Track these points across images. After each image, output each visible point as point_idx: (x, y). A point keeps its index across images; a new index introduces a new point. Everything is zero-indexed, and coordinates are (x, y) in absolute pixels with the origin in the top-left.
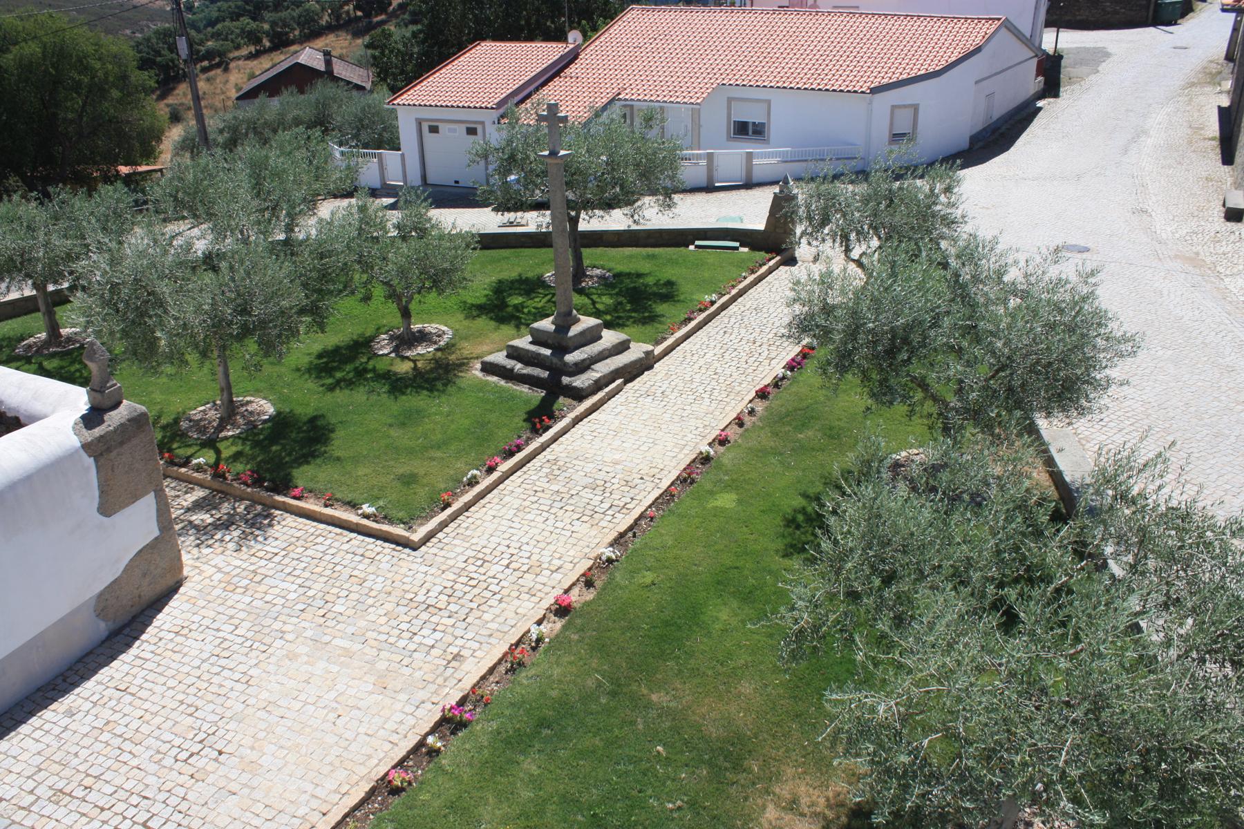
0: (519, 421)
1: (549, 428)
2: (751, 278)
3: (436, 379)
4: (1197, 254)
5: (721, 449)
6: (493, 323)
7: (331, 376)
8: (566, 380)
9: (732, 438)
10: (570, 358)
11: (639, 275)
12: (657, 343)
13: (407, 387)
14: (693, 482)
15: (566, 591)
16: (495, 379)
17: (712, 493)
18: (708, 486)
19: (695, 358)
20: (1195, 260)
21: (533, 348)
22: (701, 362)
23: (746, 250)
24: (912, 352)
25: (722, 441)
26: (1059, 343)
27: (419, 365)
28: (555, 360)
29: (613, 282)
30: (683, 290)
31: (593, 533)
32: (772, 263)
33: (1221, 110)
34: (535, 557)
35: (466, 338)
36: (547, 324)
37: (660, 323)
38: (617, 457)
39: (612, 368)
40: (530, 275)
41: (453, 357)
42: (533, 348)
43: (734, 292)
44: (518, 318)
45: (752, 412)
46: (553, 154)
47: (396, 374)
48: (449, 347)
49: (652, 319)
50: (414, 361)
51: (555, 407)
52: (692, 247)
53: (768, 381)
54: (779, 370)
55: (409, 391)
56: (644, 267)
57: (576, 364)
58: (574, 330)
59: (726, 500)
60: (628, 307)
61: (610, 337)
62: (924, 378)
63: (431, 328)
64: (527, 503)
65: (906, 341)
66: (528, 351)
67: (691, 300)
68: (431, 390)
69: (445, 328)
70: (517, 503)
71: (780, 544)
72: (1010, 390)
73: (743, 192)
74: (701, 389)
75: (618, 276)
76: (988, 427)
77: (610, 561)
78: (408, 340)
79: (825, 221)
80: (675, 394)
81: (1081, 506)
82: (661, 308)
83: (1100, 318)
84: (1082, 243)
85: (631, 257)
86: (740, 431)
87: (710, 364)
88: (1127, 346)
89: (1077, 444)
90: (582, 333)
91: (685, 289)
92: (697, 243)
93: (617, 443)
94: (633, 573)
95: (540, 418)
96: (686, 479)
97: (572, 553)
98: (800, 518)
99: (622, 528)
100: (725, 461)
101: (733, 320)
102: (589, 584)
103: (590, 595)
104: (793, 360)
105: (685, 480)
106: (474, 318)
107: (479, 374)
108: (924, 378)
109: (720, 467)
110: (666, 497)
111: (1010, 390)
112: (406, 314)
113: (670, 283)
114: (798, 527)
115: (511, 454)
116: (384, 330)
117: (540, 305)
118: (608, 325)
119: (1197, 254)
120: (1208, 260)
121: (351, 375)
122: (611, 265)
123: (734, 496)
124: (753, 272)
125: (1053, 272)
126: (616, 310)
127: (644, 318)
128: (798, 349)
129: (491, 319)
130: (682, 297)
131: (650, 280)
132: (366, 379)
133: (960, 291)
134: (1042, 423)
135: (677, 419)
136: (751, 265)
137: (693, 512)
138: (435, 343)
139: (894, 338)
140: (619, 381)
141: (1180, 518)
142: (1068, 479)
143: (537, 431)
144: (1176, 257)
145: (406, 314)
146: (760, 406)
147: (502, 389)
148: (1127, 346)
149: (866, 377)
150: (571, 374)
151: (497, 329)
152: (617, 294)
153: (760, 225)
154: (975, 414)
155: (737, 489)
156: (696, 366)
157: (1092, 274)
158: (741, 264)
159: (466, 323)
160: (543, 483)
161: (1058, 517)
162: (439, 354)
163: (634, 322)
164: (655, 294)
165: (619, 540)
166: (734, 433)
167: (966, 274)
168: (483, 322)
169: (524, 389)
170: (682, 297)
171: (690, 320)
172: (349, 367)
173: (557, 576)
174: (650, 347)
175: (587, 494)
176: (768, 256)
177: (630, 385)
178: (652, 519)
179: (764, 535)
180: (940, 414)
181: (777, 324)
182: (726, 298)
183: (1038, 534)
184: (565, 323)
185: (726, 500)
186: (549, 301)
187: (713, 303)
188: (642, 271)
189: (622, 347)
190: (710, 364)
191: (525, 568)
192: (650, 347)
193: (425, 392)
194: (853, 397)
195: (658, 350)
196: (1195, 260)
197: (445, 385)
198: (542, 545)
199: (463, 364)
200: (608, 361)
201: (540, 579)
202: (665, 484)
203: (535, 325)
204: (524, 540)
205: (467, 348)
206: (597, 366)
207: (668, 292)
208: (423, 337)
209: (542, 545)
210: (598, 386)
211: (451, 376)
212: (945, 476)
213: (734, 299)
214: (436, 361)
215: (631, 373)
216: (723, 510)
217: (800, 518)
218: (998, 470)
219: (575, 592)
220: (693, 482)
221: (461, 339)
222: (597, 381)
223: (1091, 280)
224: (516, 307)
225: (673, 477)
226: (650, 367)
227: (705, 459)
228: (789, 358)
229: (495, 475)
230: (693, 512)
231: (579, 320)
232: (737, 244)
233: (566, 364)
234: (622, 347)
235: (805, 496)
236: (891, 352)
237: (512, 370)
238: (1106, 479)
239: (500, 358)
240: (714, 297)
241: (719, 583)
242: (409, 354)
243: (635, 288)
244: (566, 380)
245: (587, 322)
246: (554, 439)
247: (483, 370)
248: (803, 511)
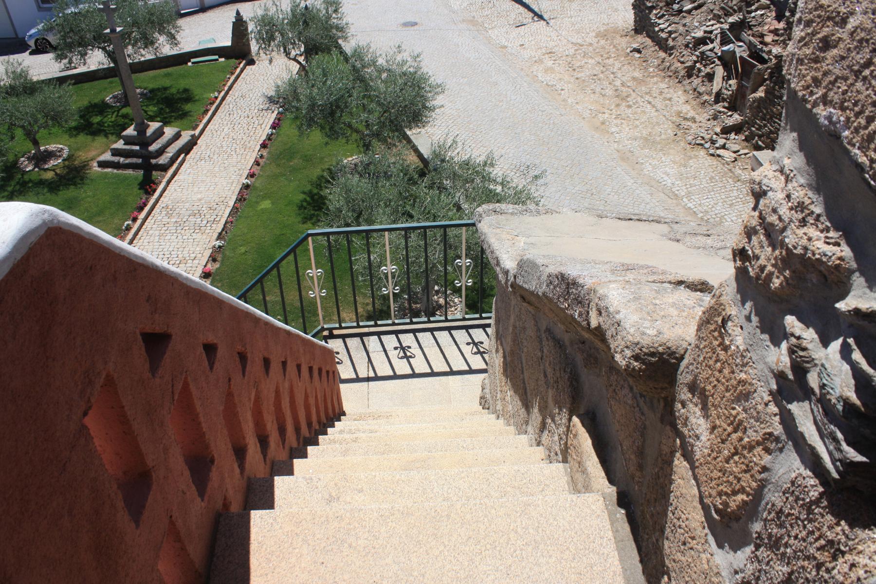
0: (136, 190)
1: (155, 191)
2: (233, 78)
3: (74, 178)
4: (474, 17)
5: (253, 180)
6: (89, 137)
7: (5, 191)
8: (153, 161)
9: (256, 173)
10: (153, 148)
11: (166, 89)
12: (194, 129)
13: (58, 186)
14: (245, 200)
15: (205, 266)
16: (110, 170)
17: (257, 203)
18: (254, 200)
19: (219, 133)
20: (473, 22)
21: (127, 147)
22: (223, 134)
23: (223, 60)
24: (342, 111)
25: (251, 175)
26: (409, 93)
27: (58, 171)
28: (143, 151)
29: (151, 95)
30: (196, 93)
31: (204, 237)
32: (242, 65)
34: (180, 256)
35: (78, 149)
36: (130, 131)
38: (199, 196)
39: (177, 149)
40: (96, 101)
41: (76, 163)
42: (127, 147)
43: (226, 88)
44: (104, 131)
45: (262, 157)
46: (113, 31)
47: (46, 180)
48: (70, 158)
49: (184, 115)
50: (54, 170)
51: (153, 178)
52: (190, 64)
53: (264, 137)
54: (268, 131)
55: (61, 188)
56: (167, 82)
57: (157, 151)
58: (149, 132)
59: (266, 204)
61: (169, 132)
62: (349, 123)
63: (52, 147)
64: (162, 232)
65: (338, 107)
66: (125, 150)
67: (204, 99)
68: (75, 184)
69: (61, 146)
70: (157, 233)
71: (299, 219)
72: (391, 121)
73: (201, 16)
74: (229, 150)
75: (152, 91)
76: (384, 141)
77: (220, 247)
78: (41, 158)
79: (272, 38)
80: (216, 156)
81: (431, 167)
82: (188, 107)
83: (424, 79)
84: (412, 20)
85: (155, 77)
86: (259, 168)
87: (229, 134)
88: (439, 89)
89: (425, 138)
90: (154, 133)
91: (197, 92)
92: (193, 60)
93: (196, 189)
94: (234, 250)
95: (148, 186)
96: (241, 199)
97: (198, 249)
98: (305, 204)
99: (220, 230)
100: (257, 185)
101: (231, 106)
102: (214, 260)
103: (217, 265)
104: (274, 123)
105: (241, 199)
106: (76, 136)
107: (97, 169)
108: (349, 123)
109: (256, 188)
110: (235, 211)
111: (391, 121)
112: (36, 143)
113: (186, 90)
114: (305, 208)
115: (141, 209)
116: (20, 155)
117: (113, 119)
118: (166, 123)
119: (474, 17)
120: (480, 20)
121: (18, 187)
122: (145, 85)
123: (269, 202)
124: (232, 74)
125: (399, 58)
126: (160, 113)
128: (274, 115)
129: (87, 134)
130: (197, 98)
131: (174, 91)
132: (29, 187)
133: (358, 77)
134: (409, 133)
135: (222, 169)
136: (230, 69)
137: (251, 214)
138: (60, 156)
139: (332, 106)
140: (183, 156)
141: (466, 164)
142: (426, 157)
143: (149, 192)
144: (464, 21)
145: (36, 143)
146: (265, 153)
147: (117, 176)
148: (439, 89)
149: (322, 128)
150: (156, 158)
151: (93, 140)
152: (157, 103)
153: (229, 43)
154: (377, 135)
155: (269, 197)
156: (221, 137)
157: (418, 56)
158: (222, 69)
159: (72, 140)
160: (166, 220)
161: (422, 174)
162: (67, 163)
164: (180, 99)
165: (220, 237)
166: (256, 169)
167: (358, 65)
168: (82, 138)
169: (130, 172)
170: (197, 98)
171: (207, 111)
172: (13, 183)
173: (196, 262)
174: (193, 133)
175: (192, 219)
176: (237, 61)
177: (188, 156)
178: (232, 222)
179: (289, 216)
180: (361, 139)
181: (257, 103)
182: (222, 94)
183: (415, 183)
184: (142, 129)
185: (266, 204)
186: (117, 116)
187: (216, 98)
188: (166, 85)
189: (177, 136)
190: (229, 134)
191: (178, 262)
192: (193, 133)
193: (72, 187)
194: (316, 136)
195: (197, 132)
196: (473, 22)
197: (82, 179)
198: (181, 249)
199: (85, 166)
200: (173, 145)
201: (188, 265)
202: (231, 204)
203: (124, 133)
204: (171, 249)
205: (83, 156)
206: (168, 149)
207: (187, 97)
208: (50, 155)
209: (181, 249)
210: (173, 160)
211: (81, 174)
212: (372, 167)
213: (227, 93)
214: (68, 167)
215: (187, 149)
216: (266, 209)
217: (305, 204)
218: (393, 160)
219: (209, 266)
220: (245, 200)
221: (76, 150)
222: (171, 158)
223: (418, 59)
224: (98, 123)
225: (234, 198)
226: (196, 144)
227: (246, 187)
228: (271, 122)
229: (139, 222)
230: (251, 214)
231: (149, 126)
232: (217, 57)
233: (150, 152)
234: (177, 136)
235: (304, 193)
236: (332, 114)
237: (119, 162)
238: (436, 155)
239: (107, 156)
240: (216, 94)
241: (277, 243)
242: (46, 167)
243: (166, 98)
244: (153, 161)
245: (154, 126)
246: (161, 196)
247: (99, 166)
248: (305, 200)
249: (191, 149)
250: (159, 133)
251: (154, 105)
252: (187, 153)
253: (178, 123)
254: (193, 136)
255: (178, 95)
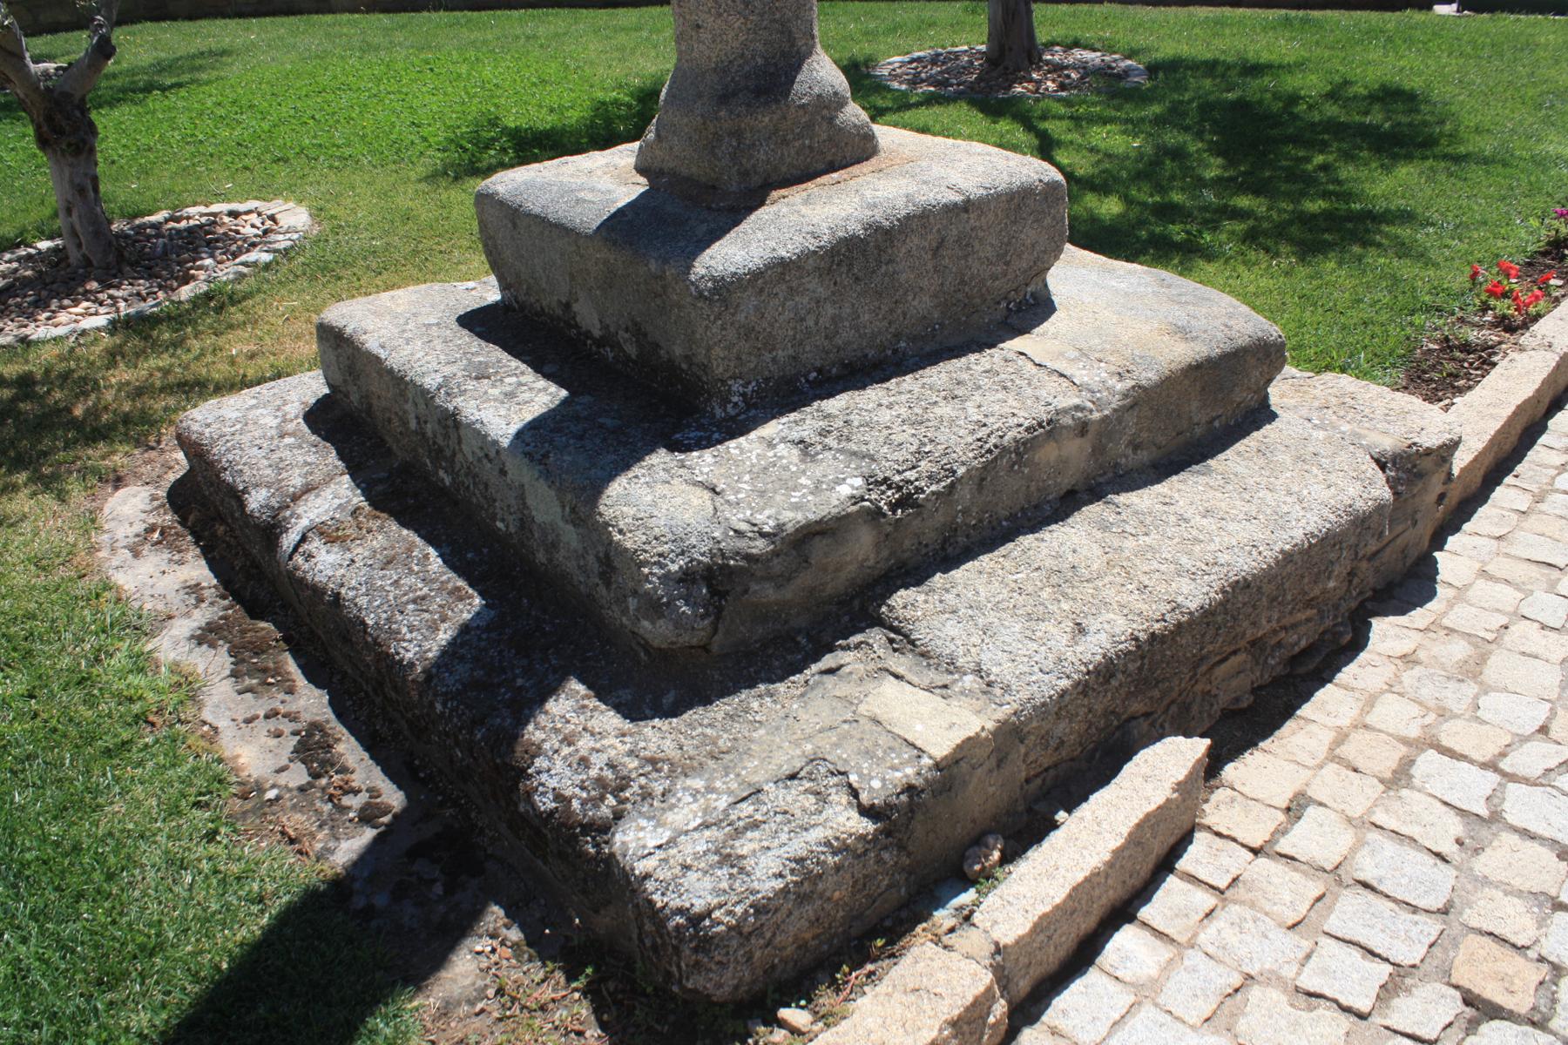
10: (669, 504)
11: (1254, 69)
12: (1442, 372)
33: (1069, 811)
37: (1404, 250)
39: (1110, 632)
49: (1344, 230)
57: (716, 580)
60: (1213, 169)
61: (1112, 322)
82: (1388, 185)
90: (857, 256)
113: (1390, 95)
127: (1306, 220)
131: (1311, 84)
140: (1167, 762)
152: (1159, 121)
163: (1251, 237)
164: (1336, 129)
177: (1262, 772)
189: (1203, 414)
192: (1426, 422)
195: (1472, 420)
200: (1073, 538)
215: (1248, 666)
226: (1409, 584)
243: (1241, 106)
249: (1337, 647)
250: (964, 290)
251: (1133, 126)
252: (1241, 726)
253: (1273, 273)
254: (1409, 468)
255: (1332, 110)
